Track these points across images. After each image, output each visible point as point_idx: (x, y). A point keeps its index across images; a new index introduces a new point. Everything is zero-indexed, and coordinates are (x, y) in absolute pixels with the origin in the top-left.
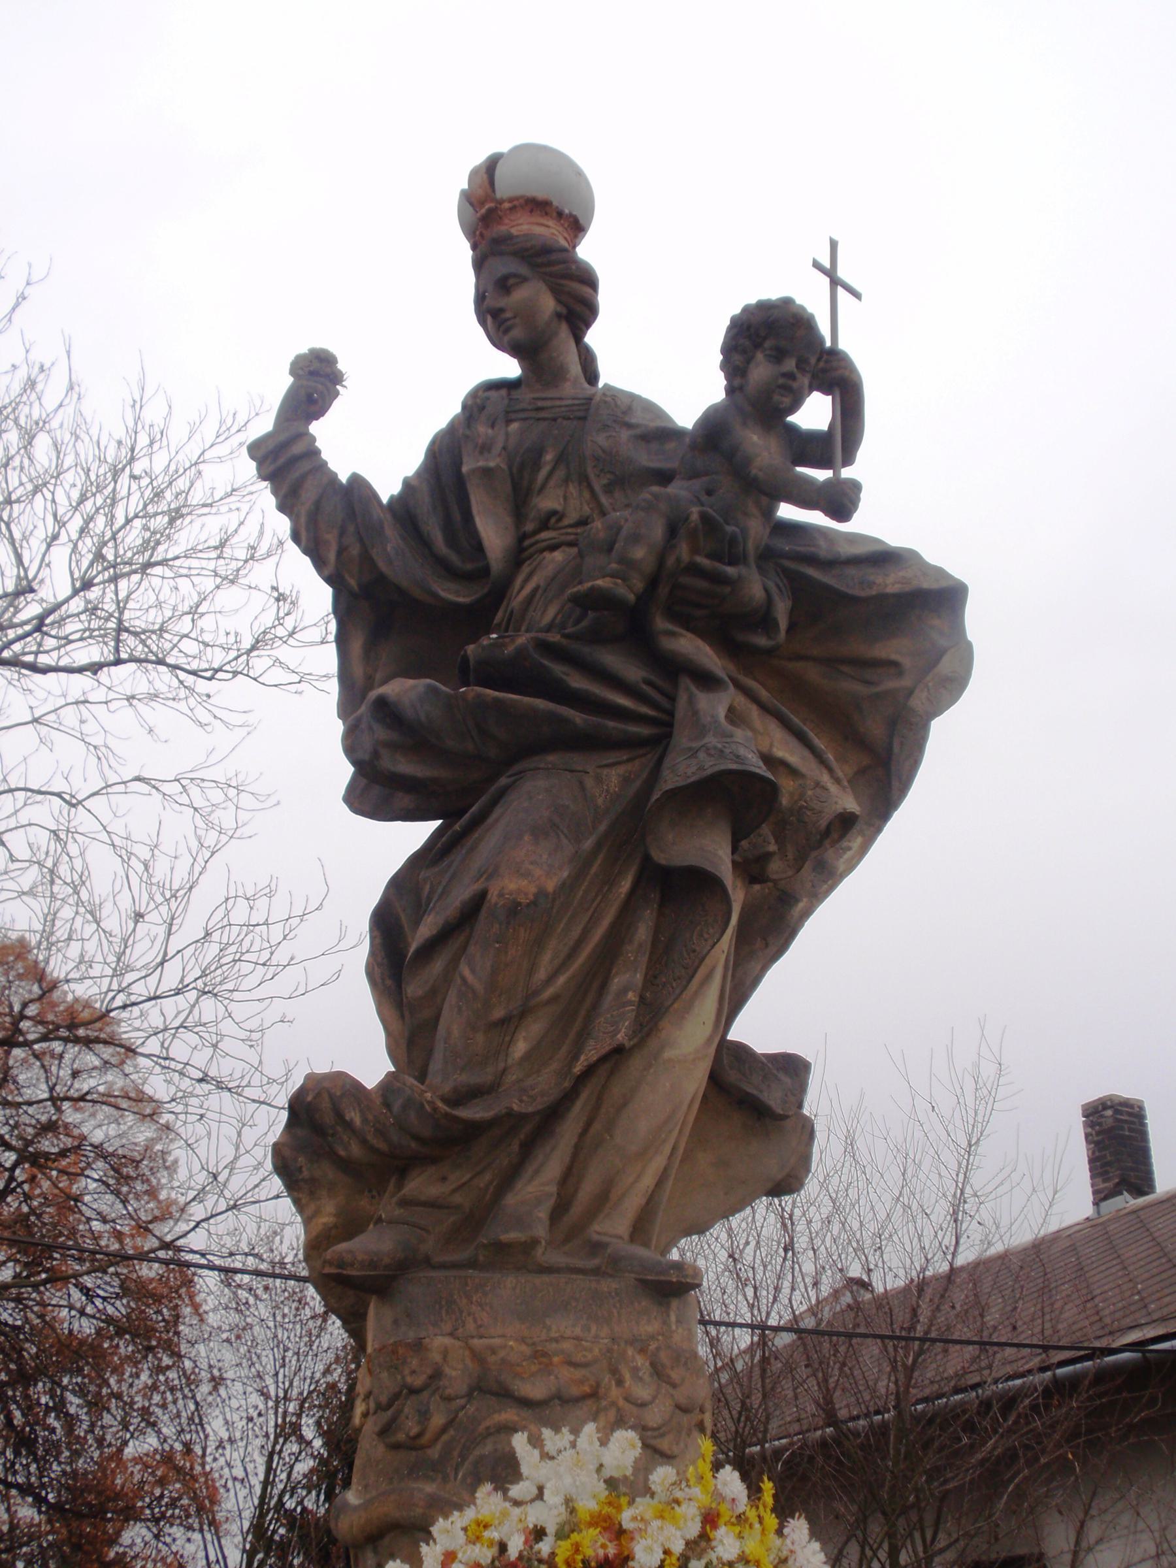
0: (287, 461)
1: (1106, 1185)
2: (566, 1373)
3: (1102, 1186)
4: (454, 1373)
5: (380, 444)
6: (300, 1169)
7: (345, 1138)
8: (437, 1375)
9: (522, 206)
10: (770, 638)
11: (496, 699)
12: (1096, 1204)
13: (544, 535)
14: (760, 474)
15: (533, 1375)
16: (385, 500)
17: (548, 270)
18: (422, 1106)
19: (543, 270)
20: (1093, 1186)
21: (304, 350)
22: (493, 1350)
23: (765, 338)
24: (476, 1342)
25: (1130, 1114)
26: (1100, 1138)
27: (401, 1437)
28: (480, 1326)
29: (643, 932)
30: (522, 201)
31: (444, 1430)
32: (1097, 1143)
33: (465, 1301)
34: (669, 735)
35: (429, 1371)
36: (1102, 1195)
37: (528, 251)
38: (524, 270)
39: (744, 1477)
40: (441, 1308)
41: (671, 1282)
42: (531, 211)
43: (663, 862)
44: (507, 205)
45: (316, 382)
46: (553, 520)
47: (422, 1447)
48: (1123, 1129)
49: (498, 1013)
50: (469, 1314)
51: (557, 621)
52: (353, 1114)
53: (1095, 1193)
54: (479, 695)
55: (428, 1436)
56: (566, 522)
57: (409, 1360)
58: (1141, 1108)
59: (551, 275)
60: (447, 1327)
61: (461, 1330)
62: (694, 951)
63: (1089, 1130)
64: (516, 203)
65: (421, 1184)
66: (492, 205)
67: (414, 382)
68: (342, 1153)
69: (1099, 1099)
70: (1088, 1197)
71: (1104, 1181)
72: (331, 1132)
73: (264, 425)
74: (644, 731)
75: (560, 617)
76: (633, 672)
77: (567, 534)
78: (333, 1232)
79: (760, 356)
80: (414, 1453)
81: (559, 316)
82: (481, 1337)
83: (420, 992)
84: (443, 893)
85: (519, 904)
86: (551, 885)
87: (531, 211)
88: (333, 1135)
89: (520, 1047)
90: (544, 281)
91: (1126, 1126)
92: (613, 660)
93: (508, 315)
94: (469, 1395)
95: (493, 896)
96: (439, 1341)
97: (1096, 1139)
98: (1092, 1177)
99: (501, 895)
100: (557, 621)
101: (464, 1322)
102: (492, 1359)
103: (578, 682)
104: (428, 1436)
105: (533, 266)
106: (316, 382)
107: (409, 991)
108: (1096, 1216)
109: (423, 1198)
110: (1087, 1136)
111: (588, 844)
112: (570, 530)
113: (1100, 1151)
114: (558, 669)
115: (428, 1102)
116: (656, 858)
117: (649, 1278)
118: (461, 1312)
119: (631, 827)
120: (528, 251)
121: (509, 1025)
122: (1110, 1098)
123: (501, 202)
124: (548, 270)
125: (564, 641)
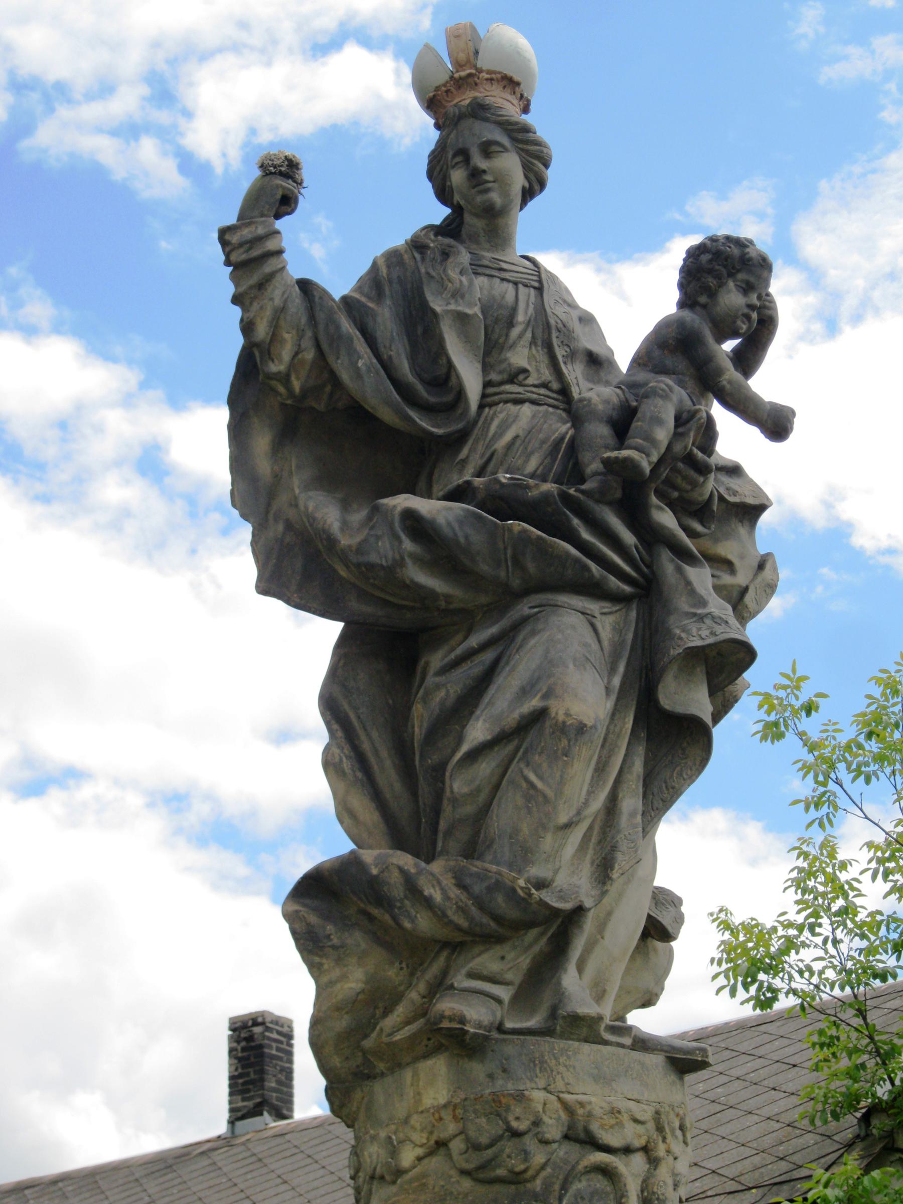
0: (249, 254)
1: (245, 1103)
3: (240, 1104)
4: (550, 1122)
6: (328, 937)
7: (413, 912)
8: (537, 1123)
9: (498, 81)
10: (704, 526)
11: (539, 538)
12: (232, 1122)
13: (508, 387)
14: (728, 386)
15: (612, 1127)
17: (525, 147)
18: (514, 890)
19: (520, 146)
20: (230, 1102)
22: (582, 1104)
23: (738, 271)
24: (566, 1097)
25: (279, 1033)
26: (245, 1054)
28: (568, 1084)
29: (638, 767)
30: (499, 76)
32: (240, 1059)
33: (554, 1062)
35: (532, 1119)
36: (239, 1114)
38: (505, 141)
40: (535, 1065)
41: (697, 1061)
42: (504, 87)
43: (667, 707)
44: (485, 75)
46: (521, 377)
47: (527, 1181)
48: (270, 1047)
50: (558, 1073)
51: (539, 472)
52: (432, 891)
53: (232, 1110)
54: (525, 531)
55: (530, 1173)
56: (530, 381)
57: (512, 1107)
58: (290, 1028)
59: (527, 152)
60: (542, 1083)
61: (553, 1086)
62: (673, 788)
63: (235, 1045)
64: (494, 76)
66: (473, 71)
68: (407, 925)
69: (251, 1014)
70: (225, 1115)
71: (244, 1100)
72: (398, 904)
75: (541, 467)
76: (628, 538)
77: (532, 392)
78: (361, 997)
80: (513, 1187)
82: (569, 1093)
83: (465, 790)
84: (488, 704)
85: (585, 725)
87: (504, 87)
88: (400, 908)
90: (520, 156)
91: (274, 1045)
93: (488, 177)
96: (538, 1096)
97: (240, 1055)
98: (231, 1094)
100: (539, 472)
101: (554, 1079)
102: (580, 1111)
104: (530, 1173)
105: (514, 140)
107: (456, 786)
108: (229, 1135)
109: (485, 973)
110: (231, 1051)
112: (534, 389)
113: (243, 1067)
115: (522, 888)
116: (662, 703)
117: (678, 1056)
118: (552, 1071)
122: (263, 1014)
123: (480, 71)
124: (525, 147)
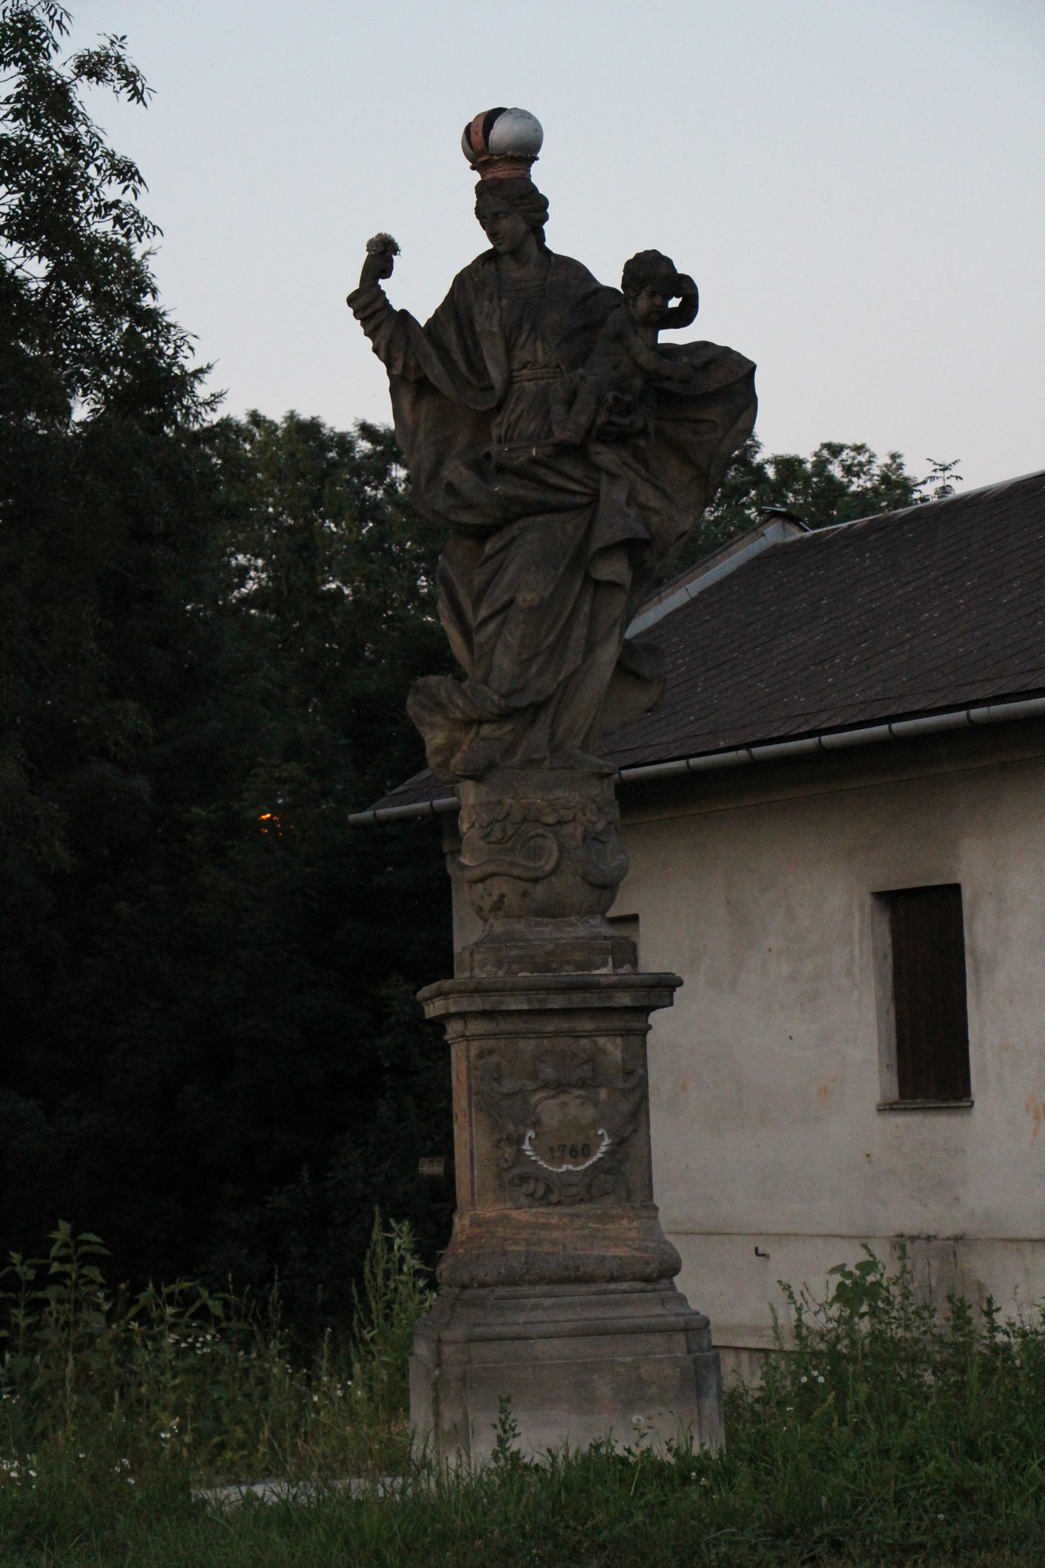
0: (369, 305)
2: (562, 812)
5: (419, 291)
16: (423, 323)
21: (373, 235)
27: (493, 839)
31: (512, 835)
34: (598, 500)
37: (503, 165)
39: (370, 1232)
45: (382, 255)
49: (525, 656)
65: (486, 730)
67: (439, 255)
73: (354, 284)
74: (584, 500)
79: (644, 293)
81: (527, 232)
86: (546, 595)
89: (534, 670)
92: (567, 467)
94: (522, 822)
95: (520, 600)
96: (508, 801)
99: (524, 601)
103: (553, 479)
106: (382, 255)
111: (562, 569)
114: (541, 471)
119: (581, 558)
120: (503, 165)
121: (529, 661)
125: (545, 459)
